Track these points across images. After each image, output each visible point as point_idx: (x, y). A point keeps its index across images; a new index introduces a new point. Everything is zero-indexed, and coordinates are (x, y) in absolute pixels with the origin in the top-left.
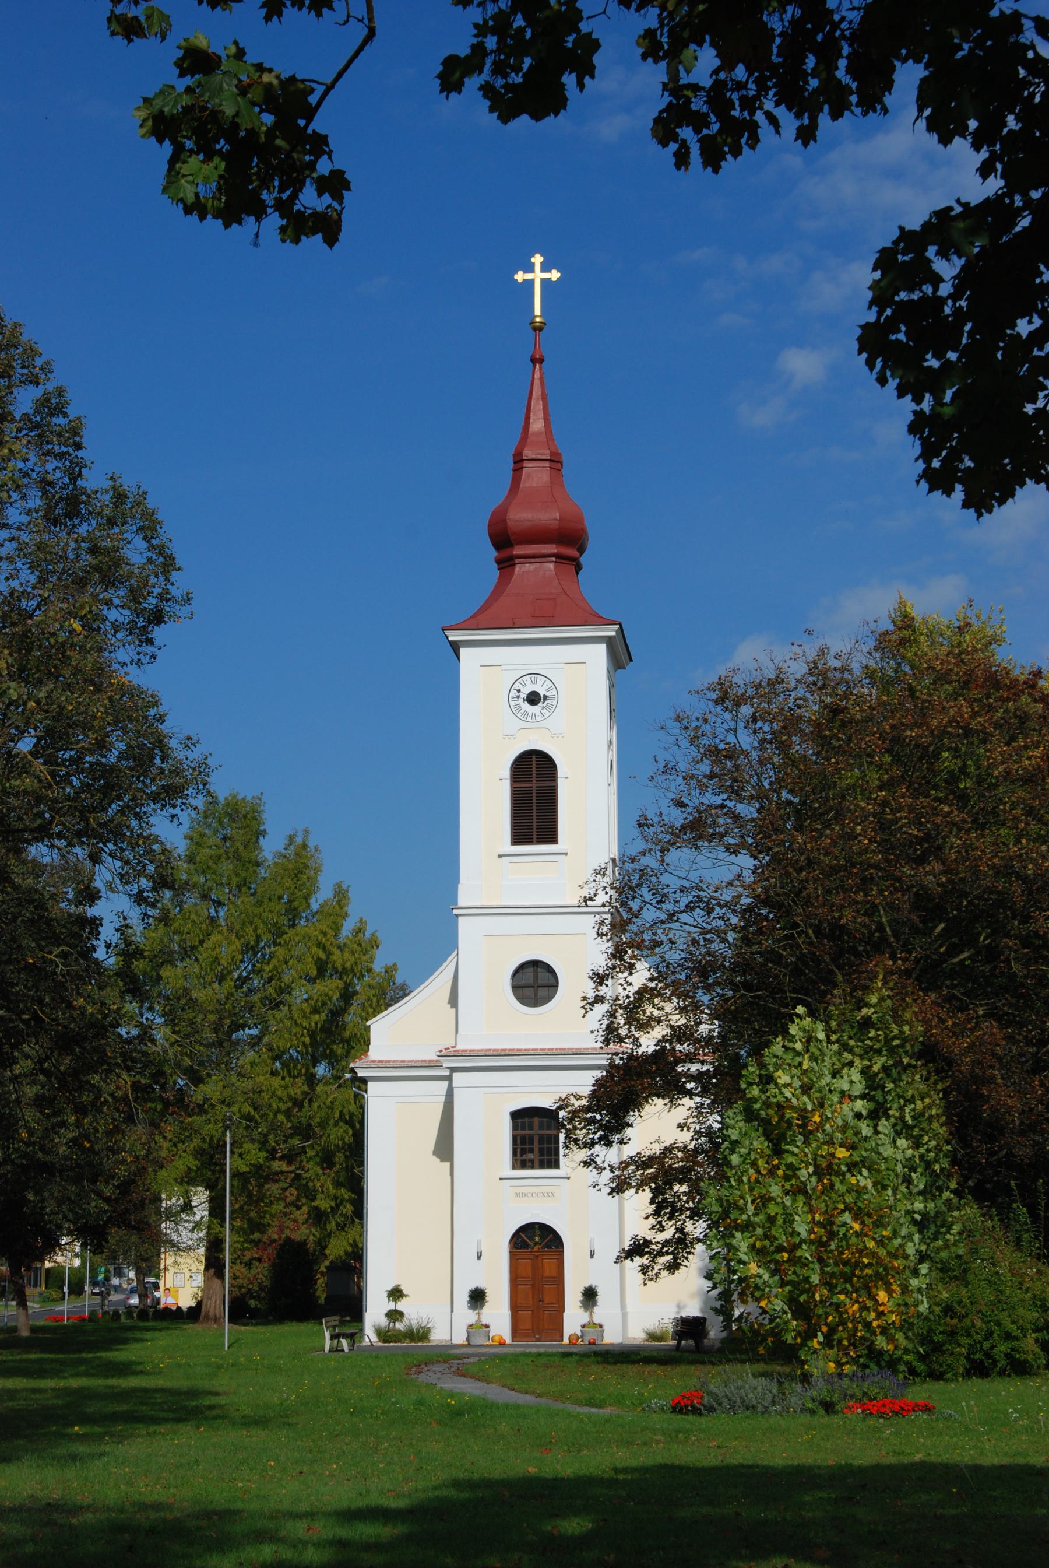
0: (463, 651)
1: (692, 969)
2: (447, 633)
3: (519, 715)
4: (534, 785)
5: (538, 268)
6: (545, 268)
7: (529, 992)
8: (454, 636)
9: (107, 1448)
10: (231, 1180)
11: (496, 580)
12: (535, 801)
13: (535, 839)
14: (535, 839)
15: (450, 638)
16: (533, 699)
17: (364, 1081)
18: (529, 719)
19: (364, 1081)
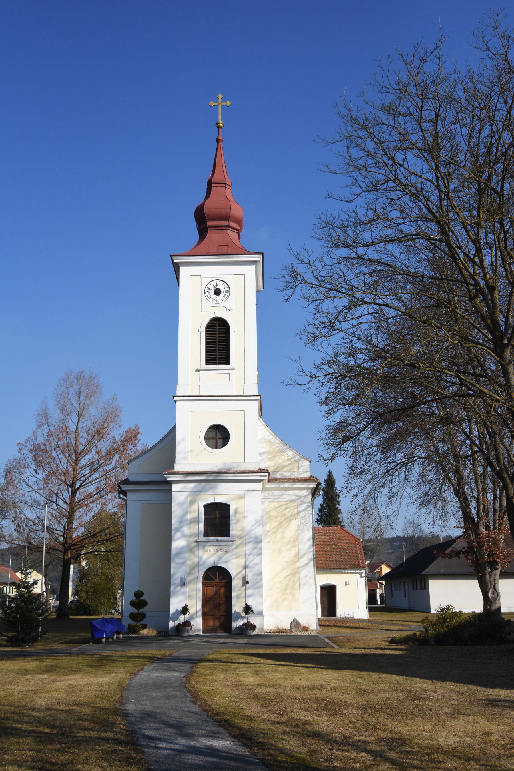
0: (182, 269)
1: (449, 363)
2: (173, 258)
3: (210, 300)
4: (218, 335)
5: (220, 100)
6: (223, 100)
7: (213, 442)
8: (176, 260)
9: (337, 339)
10: (42, 560)
11: (199, 237)
12: (218, 343)
13: (208, 516)
14: (208, 516)
15: (175, 261)
16: (217, 292)
17: (170, 483)
18: (215, 302)
19: (170, 483)
